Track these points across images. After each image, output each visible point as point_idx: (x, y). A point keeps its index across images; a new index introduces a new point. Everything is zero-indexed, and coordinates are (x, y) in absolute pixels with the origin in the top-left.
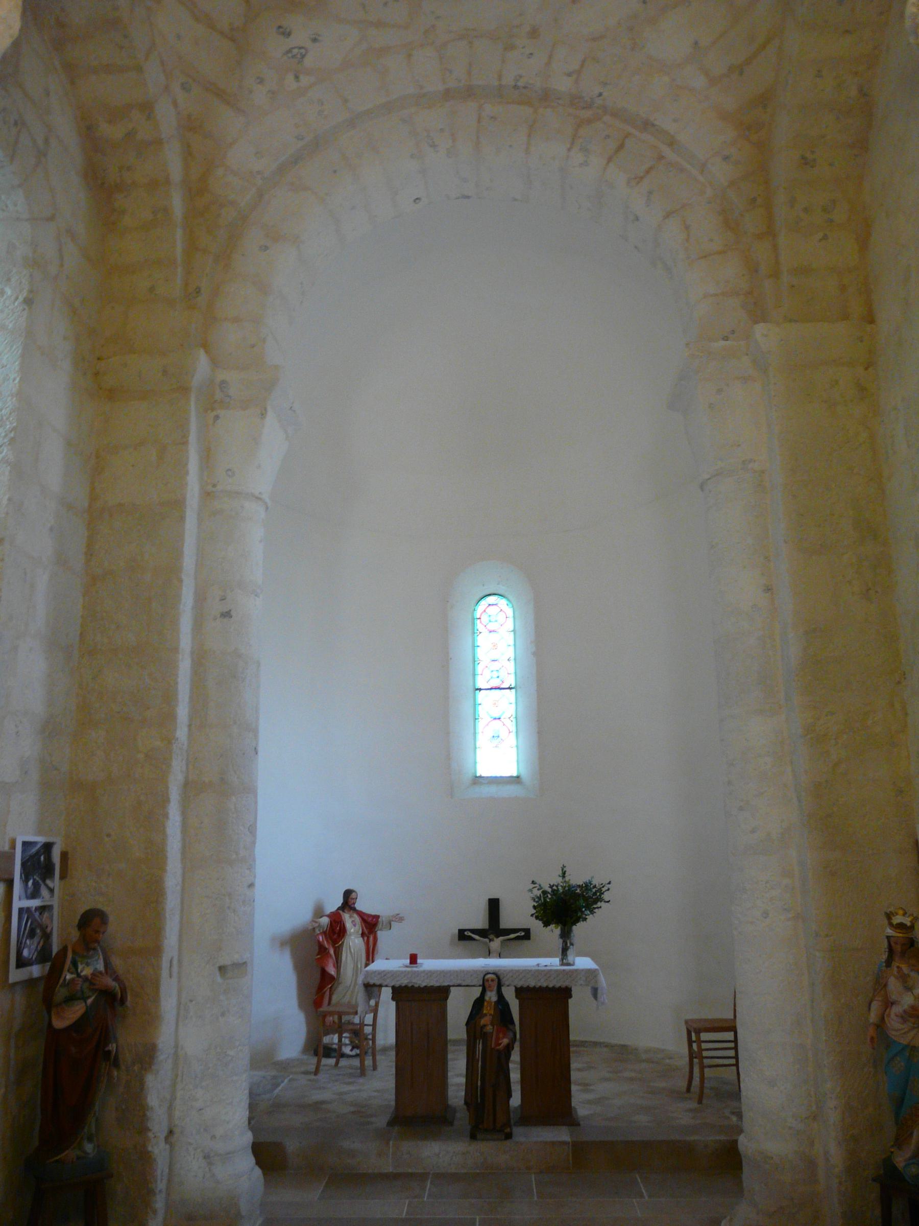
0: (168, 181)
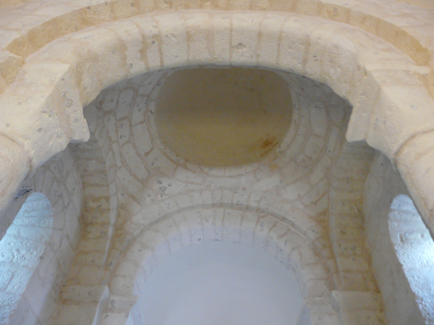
0: (109, 223)
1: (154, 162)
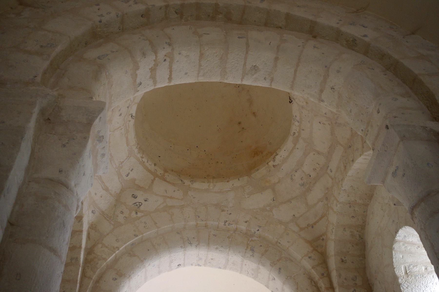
1: (129, 173)
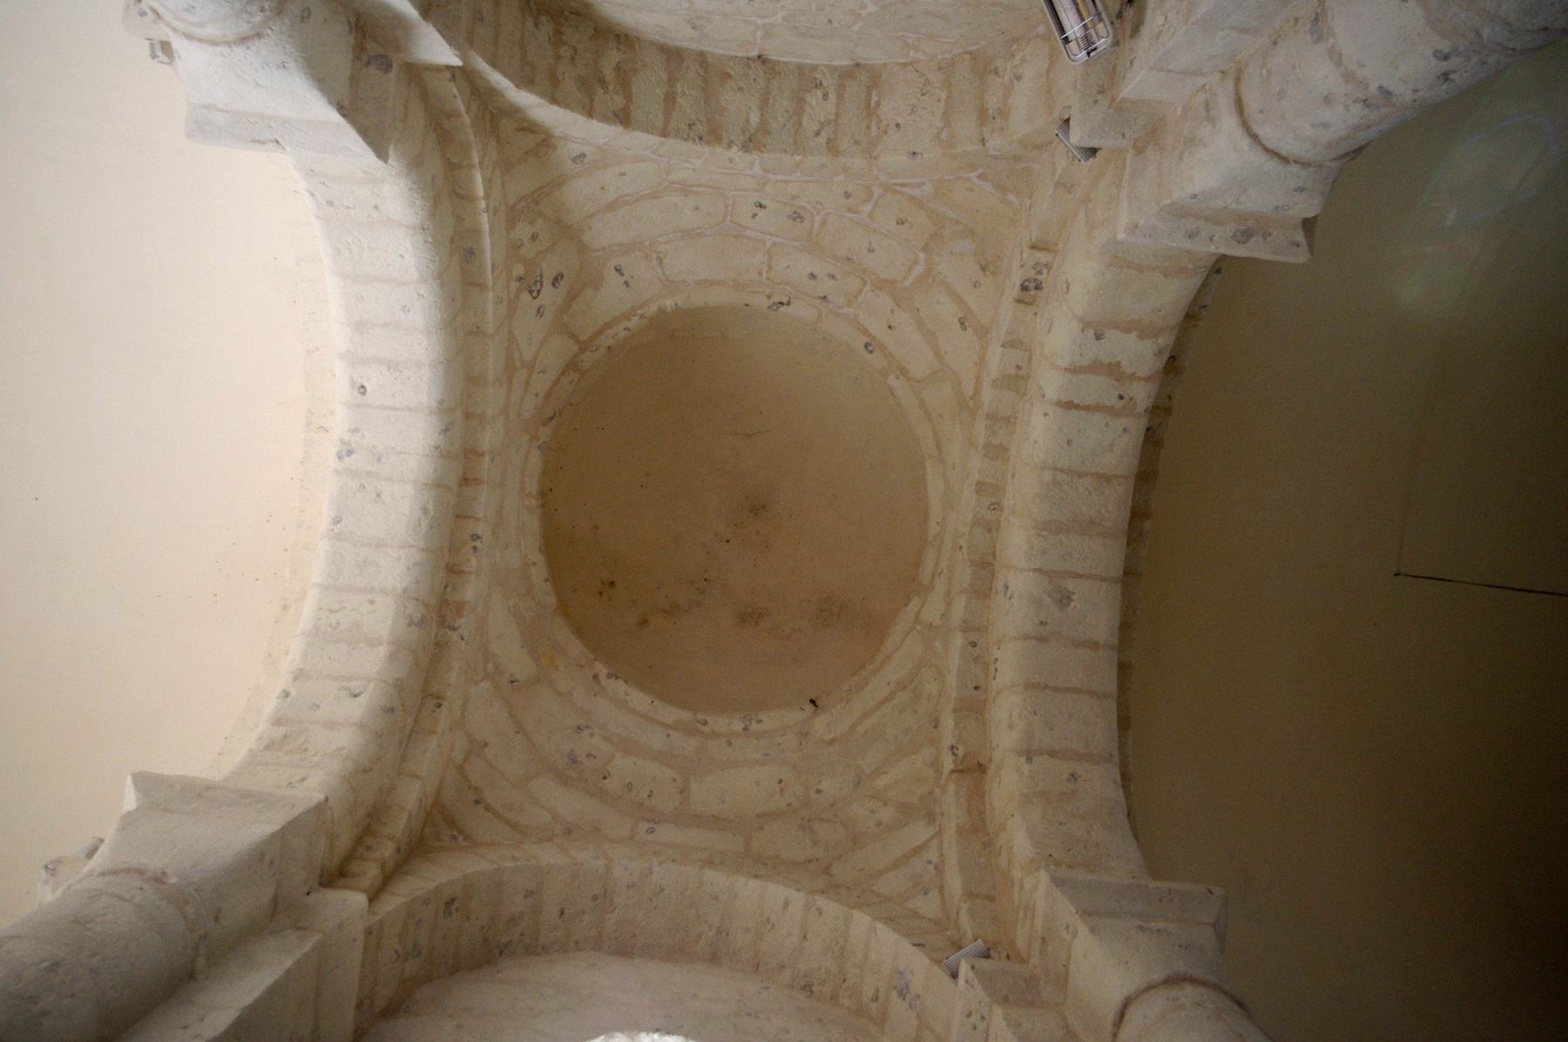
1: (622, 275)
